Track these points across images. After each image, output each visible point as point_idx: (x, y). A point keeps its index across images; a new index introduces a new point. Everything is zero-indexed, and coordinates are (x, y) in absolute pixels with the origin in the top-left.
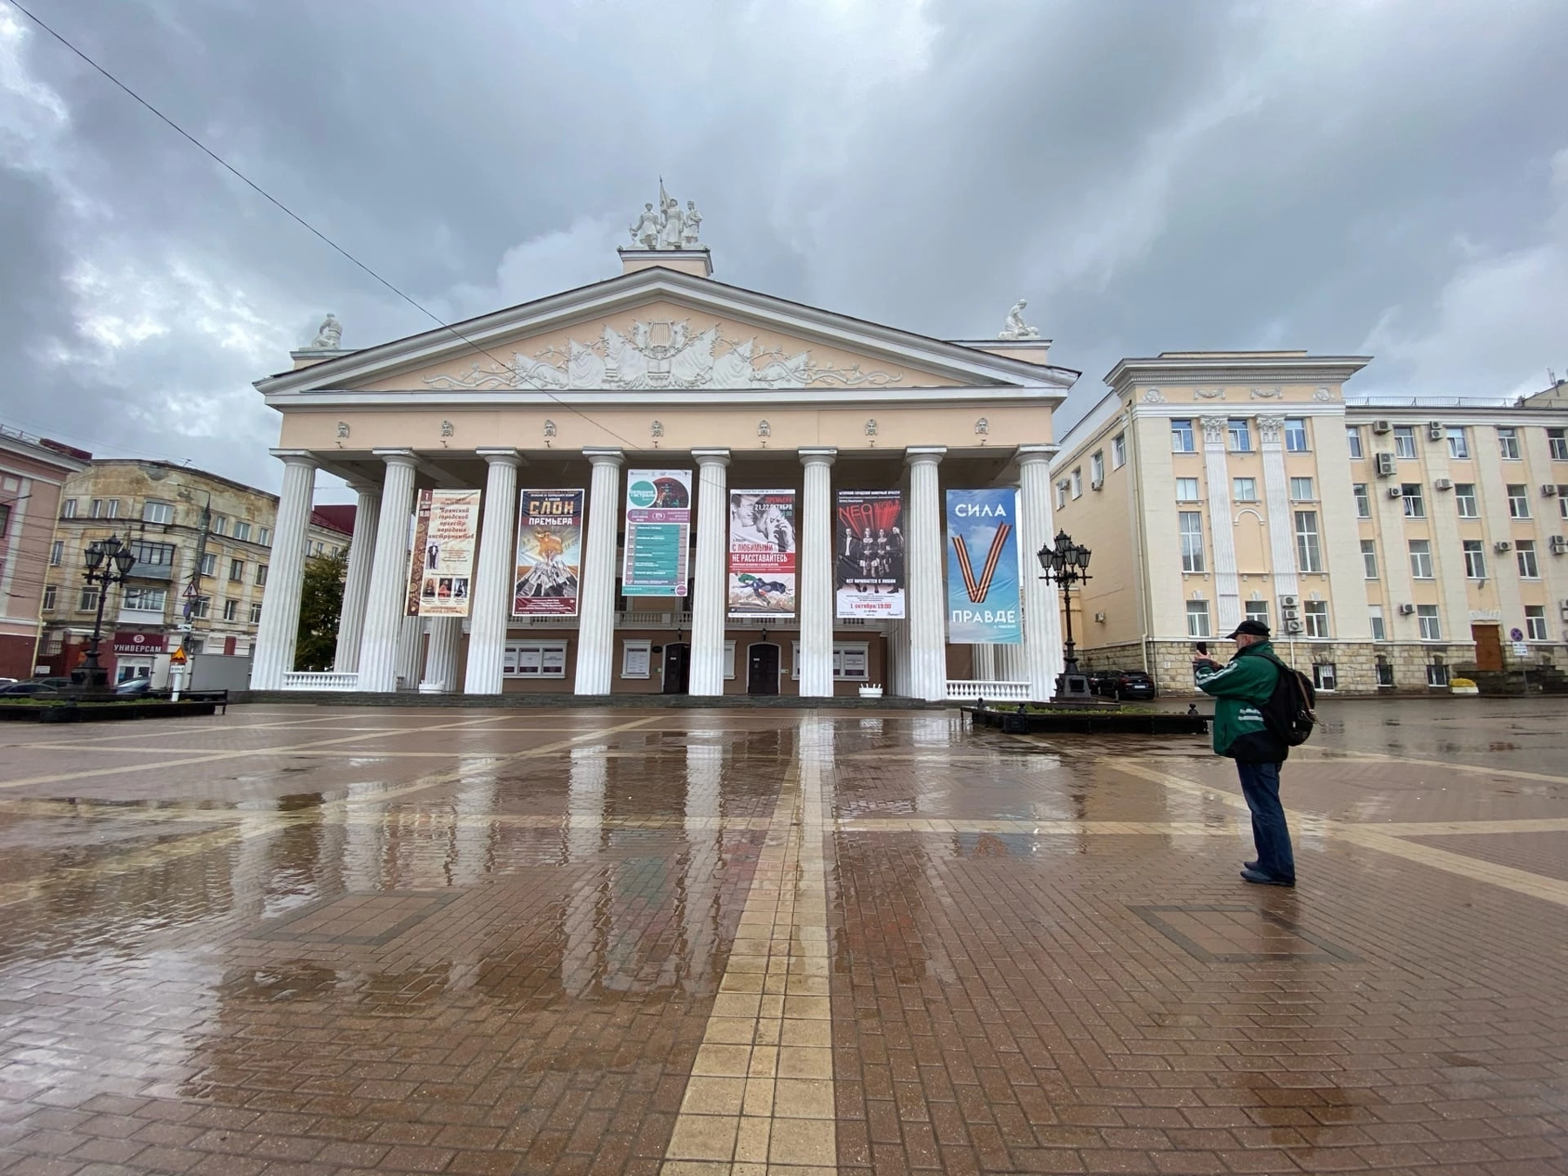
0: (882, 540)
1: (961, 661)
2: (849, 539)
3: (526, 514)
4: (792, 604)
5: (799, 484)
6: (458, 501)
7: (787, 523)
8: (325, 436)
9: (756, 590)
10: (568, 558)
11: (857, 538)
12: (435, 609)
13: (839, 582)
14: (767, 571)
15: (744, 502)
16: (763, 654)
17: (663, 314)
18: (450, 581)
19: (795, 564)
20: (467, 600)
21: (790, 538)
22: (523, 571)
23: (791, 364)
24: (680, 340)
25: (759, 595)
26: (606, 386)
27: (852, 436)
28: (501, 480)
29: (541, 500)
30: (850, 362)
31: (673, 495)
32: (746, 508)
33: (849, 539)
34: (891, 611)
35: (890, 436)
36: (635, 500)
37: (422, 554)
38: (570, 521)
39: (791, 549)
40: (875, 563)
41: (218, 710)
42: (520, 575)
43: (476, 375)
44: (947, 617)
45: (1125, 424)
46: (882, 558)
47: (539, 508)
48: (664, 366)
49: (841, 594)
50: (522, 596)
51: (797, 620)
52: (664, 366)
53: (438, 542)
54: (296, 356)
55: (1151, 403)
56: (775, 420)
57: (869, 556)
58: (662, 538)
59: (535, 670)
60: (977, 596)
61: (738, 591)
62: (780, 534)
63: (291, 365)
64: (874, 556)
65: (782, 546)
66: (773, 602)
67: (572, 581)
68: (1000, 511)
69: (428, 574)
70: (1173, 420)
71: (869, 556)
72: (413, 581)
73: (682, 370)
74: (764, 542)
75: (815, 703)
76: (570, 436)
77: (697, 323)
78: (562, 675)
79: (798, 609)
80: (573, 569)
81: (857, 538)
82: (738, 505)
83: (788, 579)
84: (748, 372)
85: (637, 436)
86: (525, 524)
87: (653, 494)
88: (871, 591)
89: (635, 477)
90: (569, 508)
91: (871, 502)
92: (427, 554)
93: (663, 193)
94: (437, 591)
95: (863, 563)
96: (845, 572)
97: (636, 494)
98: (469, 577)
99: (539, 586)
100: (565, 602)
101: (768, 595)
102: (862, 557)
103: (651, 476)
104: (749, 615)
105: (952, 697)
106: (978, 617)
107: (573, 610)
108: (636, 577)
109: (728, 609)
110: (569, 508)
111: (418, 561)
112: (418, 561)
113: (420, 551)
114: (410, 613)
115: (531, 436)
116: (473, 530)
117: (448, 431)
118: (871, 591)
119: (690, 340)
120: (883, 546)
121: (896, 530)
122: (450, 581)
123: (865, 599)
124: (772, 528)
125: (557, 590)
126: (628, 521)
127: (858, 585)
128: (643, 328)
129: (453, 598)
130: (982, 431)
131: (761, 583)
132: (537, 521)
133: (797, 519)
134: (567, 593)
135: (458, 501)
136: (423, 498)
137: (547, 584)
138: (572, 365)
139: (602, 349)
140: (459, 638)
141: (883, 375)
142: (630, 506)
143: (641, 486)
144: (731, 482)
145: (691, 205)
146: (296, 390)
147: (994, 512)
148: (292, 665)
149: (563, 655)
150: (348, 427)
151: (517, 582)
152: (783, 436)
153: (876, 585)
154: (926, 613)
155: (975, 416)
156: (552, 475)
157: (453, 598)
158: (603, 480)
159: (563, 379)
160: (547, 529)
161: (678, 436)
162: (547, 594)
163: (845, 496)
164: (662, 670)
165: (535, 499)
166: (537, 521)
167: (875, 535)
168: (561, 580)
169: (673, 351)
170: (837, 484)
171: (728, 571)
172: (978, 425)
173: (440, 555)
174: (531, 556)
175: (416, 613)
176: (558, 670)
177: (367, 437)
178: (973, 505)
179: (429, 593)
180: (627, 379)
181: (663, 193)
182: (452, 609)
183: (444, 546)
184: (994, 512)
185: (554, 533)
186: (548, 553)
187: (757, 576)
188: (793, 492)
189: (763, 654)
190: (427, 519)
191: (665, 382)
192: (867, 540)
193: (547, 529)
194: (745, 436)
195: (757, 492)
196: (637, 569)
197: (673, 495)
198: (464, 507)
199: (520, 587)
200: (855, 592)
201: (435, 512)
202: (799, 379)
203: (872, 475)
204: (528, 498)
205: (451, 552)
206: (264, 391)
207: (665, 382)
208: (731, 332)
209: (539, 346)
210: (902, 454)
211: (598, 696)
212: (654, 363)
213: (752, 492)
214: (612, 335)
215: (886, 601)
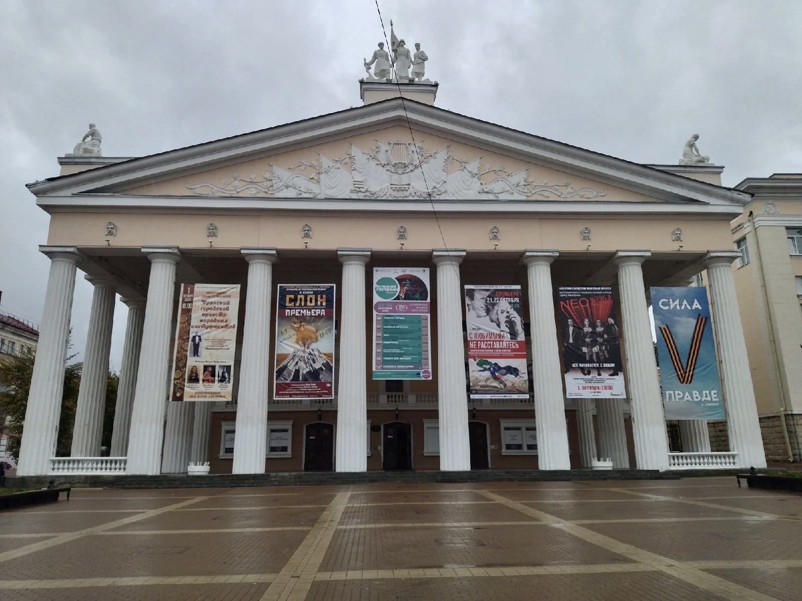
0: (600, 329)
1: (678, 436)
2: (571, 329)
3: (283, 307)
6: (218, 295)
7: (515, 314)
8: (92, 235)
9: (493, 373)
11: (578, 328)
12: (199, 394)
13: (566, 368)
14: (502, 357)
15: (478, 296)
17: (403, 136)
18: (214, 367)
19: (526, 349)
20: (230, 386)
21: (519, 327)
22: (282, 357)
23: (514, 179)
25: (496, 379)
27: (569, 241)
28: (260, 278)
30: (564, 180)
31: (414, 290)
32: (479, 300)
33: (571, 329)
34: (614, 391)
35: (603, 241)
36: (381, 294)
37: (183, 341)
39: (521, 337)
40: (596, 349)
41: (62, 496)
42: (279, 362)
43: (237, 183)
44: (663, 394)
45: (746, 231)
46: (601, 345)
47: (295, 300)
49: (569, 377)
50: (282, 381)
51: (532, 400)
52: (405, 179)
53: (202, 332)
54: (63, 162)
57: (592, 342)
59: (519, 447)
60: (685, 376)
62: (511, 324)
63: (56, 171)
64: (594, 343)
65: (514, 334)
66: (509, 384)
67: (327, 366)
68: (696, 305)
69: (191, 361)
70: (788, 228)
71: (592, 342)
72: (177, 368)
73: (418, 184)
74: (496, 331)
75: (556, 476)
76: (325, 239)
77: (430, 145)
78: (288, 454)
79: (531, 389)
80: (329, 356)
81: (578, 328)
82: (472, 298)
83: (520, 364)
85: (384, 239)
86: (282, 316)
87: (396, 289)
88: (594, 374)
89: (379, 274)
91: (588, 296)
92: (190, 343)
93: (393, 36)
94: (201, 377)
95: (585, 349)
96: (570, 358)
98: (232, 363)
99: (297, 372)
100: (322, 386)
101: (504, 378)
103: (394, 273)
104: (488, 397)
105: (673, 468)
106: (687, 397)
107: (330, 394)
108: (385, 362)
109: (469, 390)
111: (182, 349)
112: (182, 349)
114: (176, 399)
115: (289, 238)
116: (234, 320)
117: (212, 232)
118: (594, 374)
119: (426, 158)
120: (601, 335)
121: (611, 321)
122: (214, 367)
123: (590, 381)
124: (503, 319)
125: (314, 375)
126: (375, 313)
127: (582, 370)
128: (384, 147)
130: (495, 238)
131: (497, 368)
132: (293, 312)
133: (524, 309)
134: (323, 377)
135: (218, 295)
136: (186, 292)
137: (305, 370)
138: (322, 176)
139: (350, 163)
140: (222, 418)
141: (592, 192)
142: (376, 299)
143: (384, 281)
145: (418, 46)
146: (68, 192)
147: (691, 305)
148: (53, 450)
149: (289, 435)
151: (277, 367)
152: (511, 240)
156: (307, 275)
158: (353, 278)
159: (315, 189)
160: (302, 319)
161: (420, 239)
162: (305, 380)
163: (566, 291)
164: (381, 448)
166: (293, 312)
167: (593, 325)
168: (317, 366)
170: (558, 280)
172: (582, 232)
173: (203, 345)
174: (288, 345)
175: (180, 399)
177: (131, 236)
178: (675, 300)
179: (194, 379)
180: (372, 190)
181: (393, 36)
182: (217, 394)
183: (207, 336)
184: (681, 305)
186: (305, 341)
187: (493, 361)
188: (518, 287)
191: (406, 194)
192: (587, 329)
193: (302, 319)
194: (477, 240)
195: (487, 287)
196: (385, 355)
197: (414, 290)
198: (226, 300)
199: (280, 372)
200: (580, 375)
201: (197, 303)
204: (284, 293)
206: (36, 193)
207: (406, 194)
208: (460, 153)
209: (293, 160)
211: (250, 475)
212: (395, 176)
213: (483, 287)
214: (358, 151)
215: (608, 382)
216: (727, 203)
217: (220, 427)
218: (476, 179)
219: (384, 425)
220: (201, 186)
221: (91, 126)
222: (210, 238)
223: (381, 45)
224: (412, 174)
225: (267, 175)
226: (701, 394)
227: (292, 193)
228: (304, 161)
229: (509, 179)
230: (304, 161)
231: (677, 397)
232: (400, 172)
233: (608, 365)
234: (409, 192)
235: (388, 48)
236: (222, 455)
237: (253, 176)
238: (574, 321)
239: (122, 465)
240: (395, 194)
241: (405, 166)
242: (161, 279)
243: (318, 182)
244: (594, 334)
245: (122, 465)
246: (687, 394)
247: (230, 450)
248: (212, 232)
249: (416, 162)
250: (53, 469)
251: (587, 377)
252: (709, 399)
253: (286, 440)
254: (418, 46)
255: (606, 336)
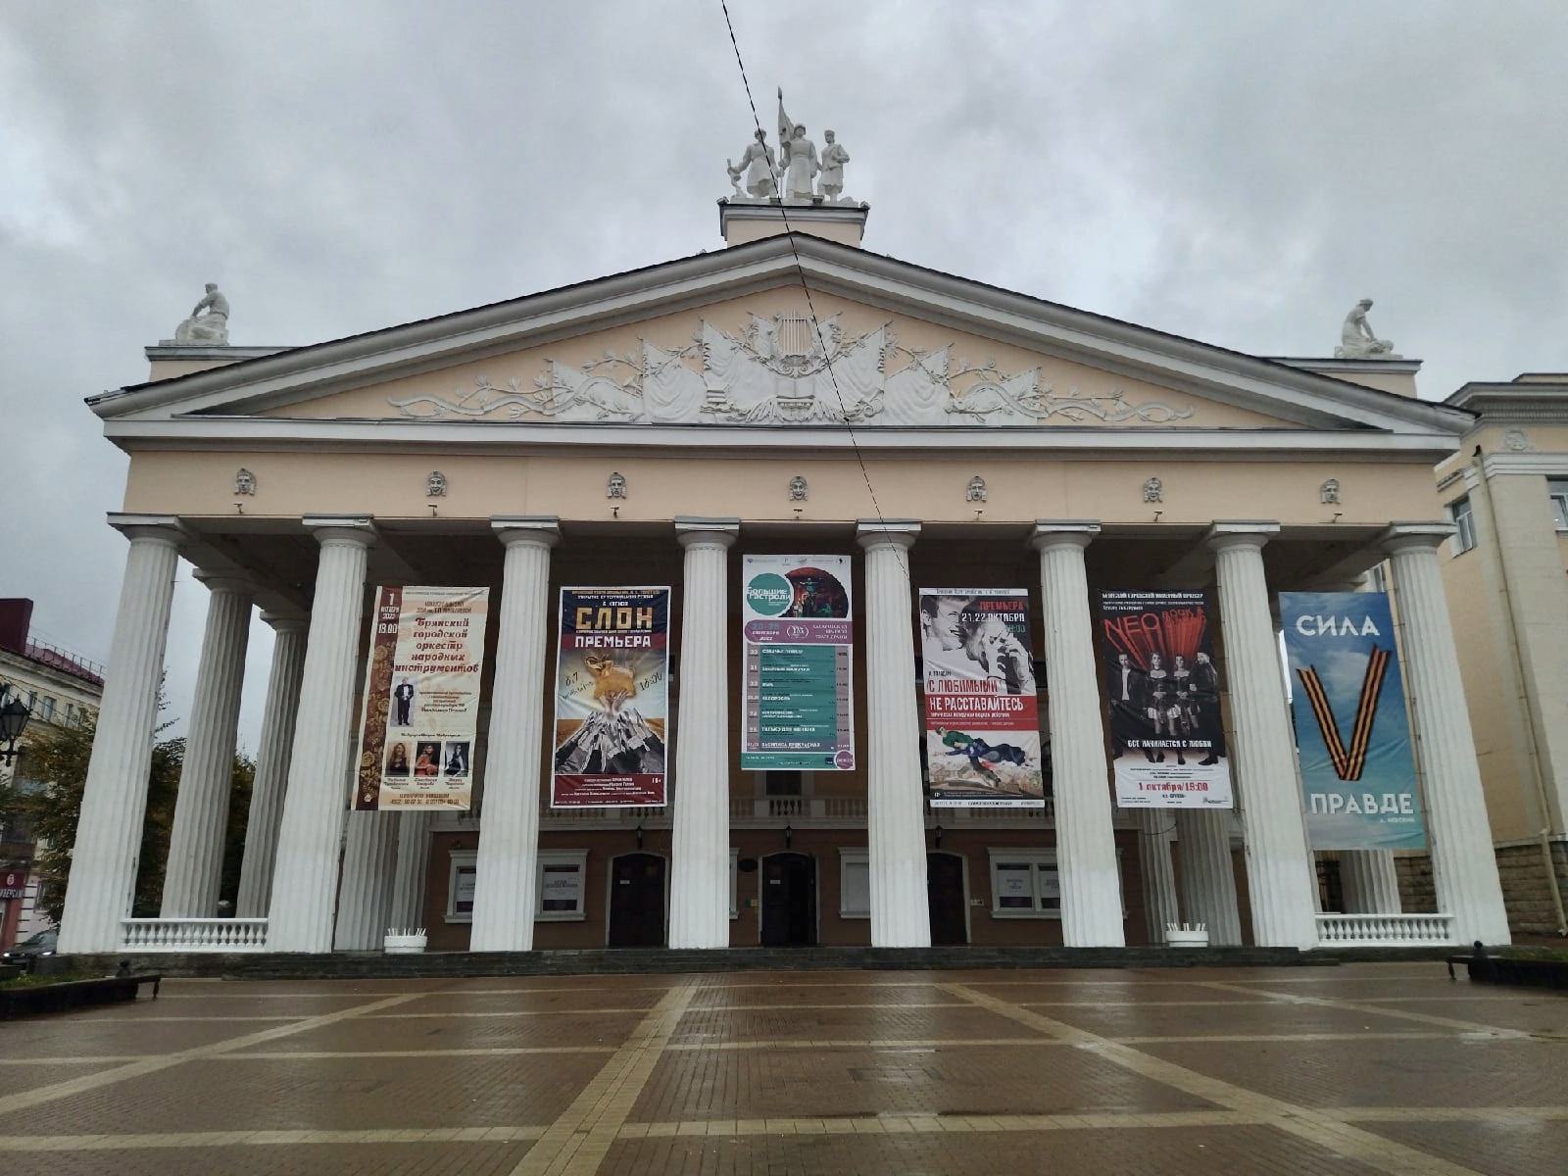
2: (1126, 672)
3: (570, 629)
4: (1038, 784)
5: (493, 579)
6: (448, 607)
8: (209, 494)
9: (974, 760)
10: (648, 704)
11: (1140, 671)
12: (411, 798)
13: (1115, 748)
15: (944, 608)
16: (985, 862)
17: (793, 305)
18: (437, 746)
19: (1037, 714)
20: (467, 782)
22: (569, 726)
24: (831, 348)
25: (980, 768)
26: (708, 419)
27: (1118, 503)
28: (526, 574)
29: (595, 604)
31: (821, 596)
34: (1210, 794)
35: (1186, 503)
37: (379, 697)
38: (647, 642)
39: (1029, 688)
40: (1174, 712)
45: (1469, 484)
46: (1184, 704)
47: (593, 618)
48: (804, 387)
49: (1118, 764)
50: (567, 772)
51: (1049, 811)
52: (804, 387)
54: (155, 355)
55: (1515, 452)
56: (636, 475)
57: (1168, 699)
58: (805, 669)
60: (1349, 769)
61: (943, 760)
62: (1008, 663)
63: (142, 372)
65: (1014, 684)
67: (654, 744)
68: (1369, 628)
69: (394, 734)
70: (1550, 478)
71: (1168, 699)
72: (367, 747)
73: (835, 392)
74: (980, 676)
75: (1095, 958)
76: (652, 500)
78: (579, 913)
79: (1048, 790)
80: (657, 724)
81: (1140, 671)
82: (933, 614)
83: (1027, 741)
84: (943, 398)
85: (763, 500)
86: (568, 646)
87: (788, 595)
89: (754, 566)
90: (645, 618)
92: (393, 700)
93: (782, 116)
94: (412, 765)
95: (1153, 713)
96: (1124, 730)
97: (757, 594)
98: (471, 737)
99: (597, 754)
100: (644, 782)
101: (996, 768)
102: (1151, 702)
103: (782, 565)
104: (965, 804)
106: (1352, 805)
107: (659, 797)
108: (766, 737)
109: (928, 792)
110: (645, 618)
111: (376, 711)
112: (376, 711)
113: (381, 694)
115: (584, 499)
116: (475, 654)
117: (799, 491)
121: (1203, 658)
122: (437, 746)
125: (629, 761)
128: (765, 326)
129: (442, 778)
131: (982, 748)
133: (1034, 634)
134: (647, 766)
135: (448, 607)
136: (385, 602)
137: (611, 750)
138: (648, 382)
141: (1164, 410)
142: (749, 615)
143: (765, 581)
144: (919, 575)
145: (830, 136)
146: (164, 413)
147: (1359, 627)
148: (128, 904)
150: (253, 479)
151: (557, 745)
152: (1008, 502)
153: (1179, 751)
154: (1272, 797)
155: (1319, 477)
156: (616, 569)
157: (442, 778)
159: (634, 407)
160: (606, 654)
161: (833, 500)
164: (758, 903)
165: (586, 603)
167: (1168, 665)
168: (634, 743)
169: (817, 364)
171: (924, 725)
173: (417, 702)
174: (580, 702)
175: (373, 805)
176: (1001, 867)
177: (283, 496)
178: (1327, 618)
179: (399, 768)
181: (782, 116)
182: (441, 798)
183: (424, 683)
184: (1338, 628)
185: (620, 661)
186: (612, 696)
187: (974, 735)
188: (1024, 592)
189: (985, 862)
190: (393, 637)
191: (808, 414)
192: (1158, 674)
195: (964, 592)
198: (460, 617)
199: (563, 756)
201: (407, 625)
202: (1025, 411)
203: (1153, 570)
204: (572, 602)
205: (437, 695)
206: (104, 415)
207: (808, 414)
208: (909, 336)
210: (1029, 530)
212: (786, 382)
213: (954, 592)
214: (716, 333)
216: (1428, 431)
217: (449, 860)
218: (939, 386)
219: (615, 860)
220: (374, 406)
221: (209, 288)
222: (241, 496)
223: (760, 134)
224: (817, 377)
225: (542, 380)
226: (1378, 799)
227: (588, 414)
228: (612, 353)
229: (1005, 385)
230: (612, 353)
231: (1333, 806)
232: (795, 373)
233: (1194, 744)
234: (811, 411)
235: (773, 140)
236: (451, 916)
237: (514, 381)
238: (1130, 657)
239: (259, 935)
240: (786, 414)
241: (805, 362)
242: (339, 577)
243: (640, 392)
244: (1169, 683)
245: (259, 935)
246: (1352, 800)
247: (467, 907)
248: (799, 491)
249: (830, 353)
250: (127, 941)
251: (1161, 766)
252: (1395, 809)
253: (575, 888)
254: (830, 136)
255: (1193, 687)
